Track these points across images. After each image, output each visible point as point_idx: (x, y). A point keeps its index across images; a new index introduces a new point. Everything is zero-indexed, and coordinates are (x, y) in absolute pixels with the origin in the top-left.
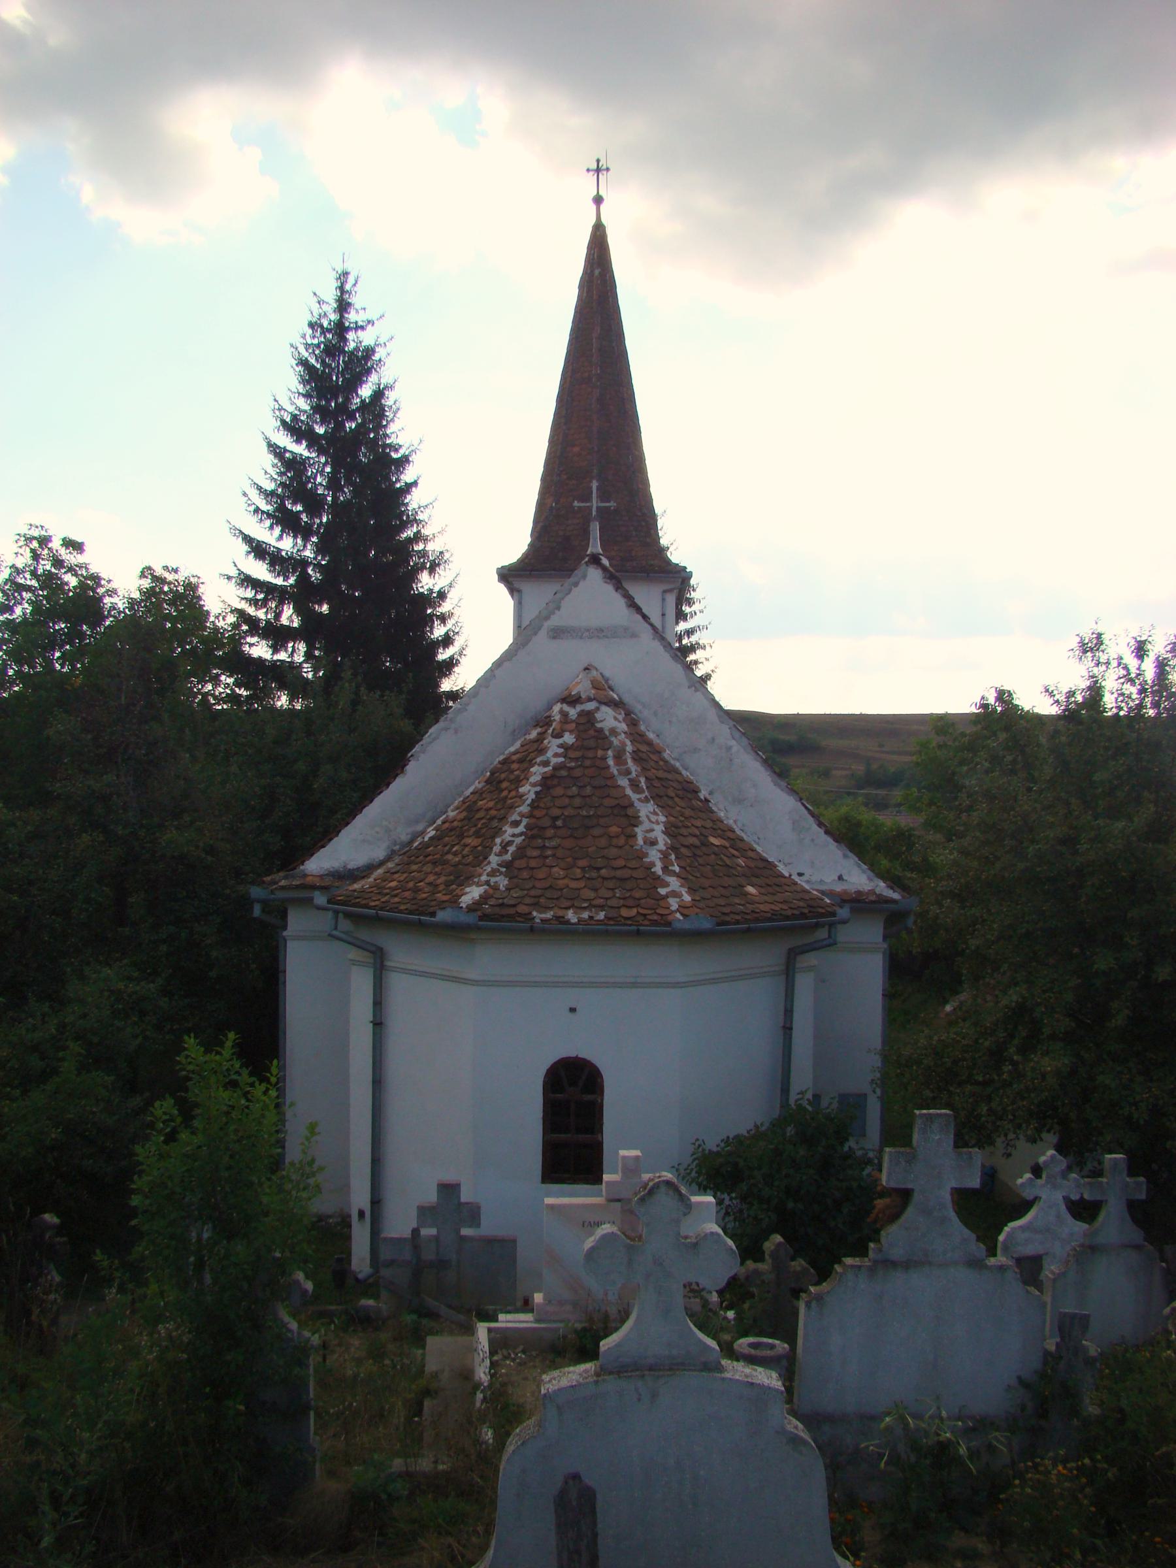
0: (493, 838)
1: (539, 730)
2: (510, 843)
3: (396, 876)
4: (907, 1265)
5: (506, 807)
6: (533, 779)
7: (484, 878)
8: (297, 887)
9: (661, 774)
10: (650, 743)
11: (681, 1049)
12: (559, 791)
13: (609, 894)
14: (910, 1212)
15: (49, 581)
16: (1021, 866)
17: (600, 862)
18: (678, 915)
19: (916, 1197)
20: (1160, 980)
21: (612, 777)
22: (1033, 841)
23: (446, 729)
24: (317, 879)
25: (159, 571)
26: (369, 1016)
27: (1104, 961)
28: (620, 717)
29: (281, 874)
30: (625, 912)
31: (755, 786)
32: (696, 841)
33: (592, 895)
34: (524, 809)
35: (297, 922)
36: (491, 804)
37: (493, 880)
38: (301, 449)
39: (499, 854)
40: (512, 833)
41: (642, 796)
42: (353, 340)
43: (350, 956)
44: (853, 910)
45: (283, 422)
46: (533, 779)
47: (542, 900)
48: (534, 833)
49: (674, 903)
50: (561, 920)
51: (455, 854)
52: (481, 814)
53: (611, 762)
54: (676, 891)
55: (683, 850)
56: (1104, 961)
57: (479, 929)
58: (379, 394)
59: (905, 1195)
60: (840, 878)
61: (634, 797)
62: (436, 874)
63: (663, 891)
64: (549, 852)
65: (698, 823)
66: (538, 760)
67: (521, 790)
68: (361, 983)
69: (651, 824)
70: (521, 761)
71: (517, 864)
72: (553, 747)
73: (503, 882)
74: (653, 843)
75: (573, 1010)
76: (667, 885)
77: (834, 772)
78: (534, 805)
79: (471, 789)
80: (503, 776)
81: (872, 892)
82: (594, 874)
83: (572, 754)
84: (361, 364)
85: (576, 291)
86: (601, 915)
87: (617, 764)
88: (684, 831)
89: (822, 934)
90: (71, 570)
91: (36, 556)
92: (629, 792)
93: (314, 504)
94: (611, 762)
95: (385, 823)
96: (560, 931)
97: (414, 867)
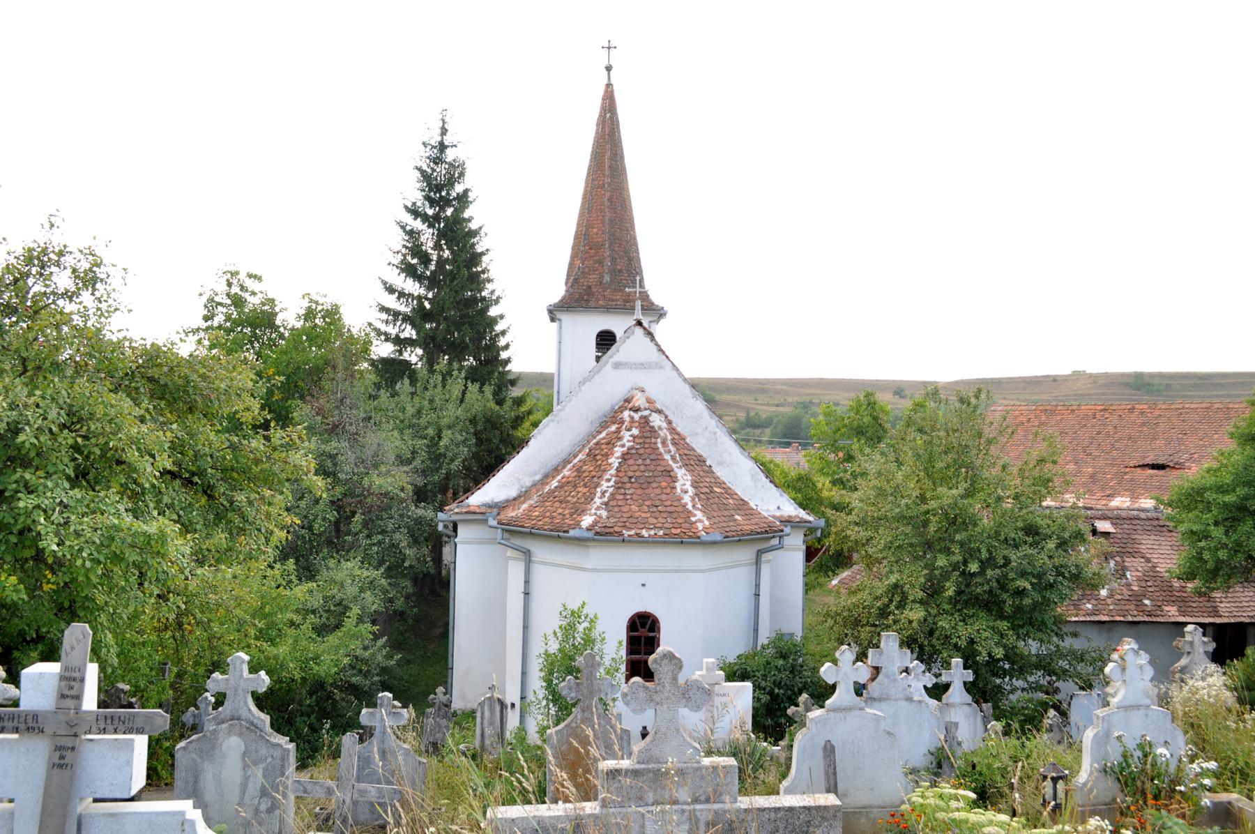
4: (880, 700)
5: (601, 470)
7: (593, 511)
10: (679, 434)
11: (710, 608)
12: (631, 462)
14: (880, 677)
15: (238, 302)
16: (897, 510)
17: (657, 503)
19: (883, 670)
25: (315, 298)
26: (521, 587)
27: (942, 561)
29: (455, 505)
30: (674, 531)
34: (613, 472)
38: (418, 224)
40: (607, 486)
42: (450, 155)
45: (406, 207)
48: (619, 486)
49: (700, 526)
53: (660, 445)
54: (700, 520)
56: (942, 561)
57: (594, 540)
58: (466, 191)
61: (674, 466)
63: (693, 519)
68: (516, 570)
69: (684, 480)
70: (607, 444)
72: (627, 436)
73: (604, 514)
78: (618, 470)
84: (456, 172)
86: (661, 533)
89: (775, 542)
90: (253, 293)
91: (229, 284)
92: (671, 462)
93: (425, 259)
94: (660, 445)
96: (639, 541)
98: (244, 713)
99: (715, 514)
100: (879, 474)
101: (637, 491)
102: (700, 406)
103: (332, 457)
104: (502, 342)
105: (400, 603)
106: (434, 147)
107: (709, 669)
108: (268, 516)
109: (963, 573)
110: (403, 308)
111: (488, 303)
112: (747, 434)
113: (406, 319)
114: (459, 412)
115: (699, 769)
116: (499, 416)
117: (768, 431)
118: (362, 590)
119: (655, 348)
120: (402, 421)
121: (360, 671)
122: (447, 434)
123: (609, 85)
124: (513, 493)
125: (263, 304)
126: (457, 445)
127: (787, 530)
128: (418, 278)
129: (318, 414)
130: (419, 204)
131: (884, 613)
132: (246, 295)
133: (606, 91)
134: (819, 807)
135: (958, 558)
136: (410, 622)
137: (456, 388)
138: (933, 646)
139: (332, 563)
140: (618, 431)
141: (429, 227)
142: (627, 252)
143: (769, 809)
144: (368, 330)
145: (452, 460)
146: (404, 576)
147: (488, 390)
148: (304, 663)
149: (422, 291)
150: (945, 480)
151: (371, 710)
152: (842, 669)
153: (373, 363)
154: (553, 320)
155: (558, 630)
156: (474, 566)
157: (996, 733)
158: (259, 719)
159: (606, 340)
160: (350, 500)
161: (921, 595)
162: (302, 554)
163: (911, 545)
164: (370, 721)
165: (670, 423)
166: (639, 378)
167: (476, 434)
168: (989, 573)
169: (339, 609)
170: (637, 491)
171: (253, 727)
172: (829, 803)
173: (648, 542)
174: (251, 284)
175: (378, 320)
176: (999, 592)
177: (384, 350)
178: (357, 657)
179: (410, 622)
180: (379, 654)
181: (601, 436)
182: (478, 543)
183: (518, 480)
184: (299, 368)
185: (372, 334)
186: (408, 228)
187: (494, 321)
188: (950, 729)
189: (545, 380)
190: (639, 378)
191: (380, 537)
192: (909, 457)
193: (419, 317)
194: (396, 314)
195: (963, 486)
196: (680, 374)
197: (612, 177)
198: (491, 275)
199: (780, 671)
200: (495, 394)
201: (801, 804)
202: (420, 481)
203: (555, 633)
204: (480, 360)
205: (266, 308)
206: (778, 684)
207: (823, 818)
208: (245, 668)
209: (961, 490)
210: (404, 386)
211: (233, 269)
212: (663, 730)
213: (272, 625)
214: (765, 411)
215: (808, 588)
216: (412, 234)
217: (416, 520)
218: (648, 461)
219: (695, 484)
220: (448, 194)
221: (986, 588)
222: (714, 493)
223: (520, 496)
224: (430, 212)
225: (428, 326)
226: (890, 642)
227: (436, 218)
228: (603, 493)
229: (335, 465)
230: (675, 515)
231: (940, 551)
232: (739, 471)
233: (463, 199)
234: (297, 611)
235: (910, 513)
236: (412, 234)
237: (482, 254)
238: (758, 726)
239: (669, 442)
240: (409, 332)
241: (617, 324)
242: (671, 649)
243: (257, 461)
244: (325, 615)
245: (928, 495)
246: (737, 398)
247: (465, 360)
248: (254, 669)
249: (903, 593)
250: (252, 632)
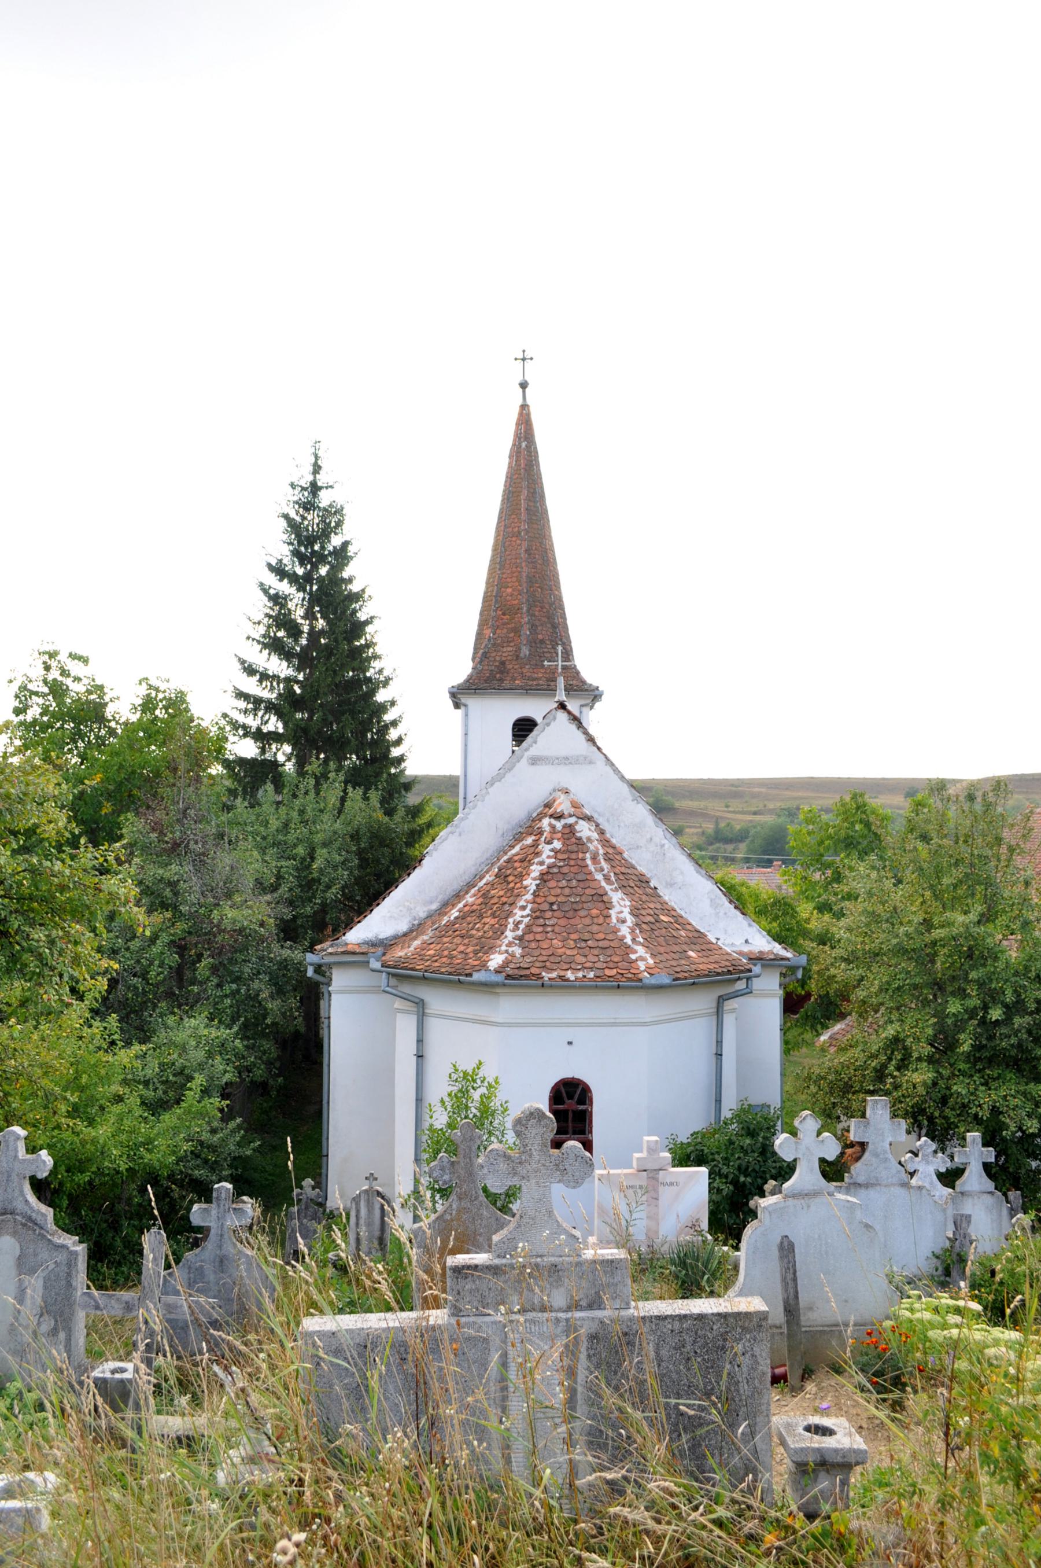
0: (506, 918)
1: (533, 838)
2: (519, 922)
3: (432, 946)
4: (867, 1186)
6: (533, 875)
7: (504, 948)
8: (343, 953)
9: (623, 870)
10: (614, 847)
11: (652, 1069)
12: (552, 884)
13: (596, 959)
14: (867, 1155)
15: (57, 690)
16: (894, 941)
17: (587, 936)
18: (646, 974)
19: (870, 1147)
20: (993, 1019)
21: (591, 873)
22: (901, 924)
23: (452, 833)
24: (356, 947)
25: (153, 682)
27: (954, 1007)
28: (593, 828)
29: (328, 943)
30: (608, 972)
31: (682, 873)
32: (650, 919)
33: (584, 960)
34: (529, 897)
35: (339, 979)
36: (502, 893)
37: (510, 950)
38: (284, 587)
39: (513, 931)
40: (521, 915)
41: (613, 887)
42: (325, 499)
43: (395, 1006)
44: (763, 966)
45: (269, 566)
46: (533, 875)
47: (548, 964)
48: (537, 915)
49: (642, 965)
50: (562, 978)
51: (478, 930)
52: (495, 900)
53: (589, 862)
54: (642, 957)
55: (644, 926)
56: (954, 1007)
57: (504, 985)
58: (346, 544)
59: (863, 1145)
60: (747, 941)
61: (608, 888)
62: (464, 945)
63: (633, 957)
64: (549, 929)
65: (652, 905)
66: (536, 860)
67: (525, 883)
68: (406, 1026)
69: (621, 906)
70: (522, 861)
71: (527, 937)
72: (546, 850)
73: (518, 951)
74: (624, 922)
75: (570, 1043)
76: (636, 952)
77: (687, 830)
78: (535, 894)
79: (484, 881)
80: (509, 872)
81: (771, 952)
82: (583, 945)
83: (560, 856)
84: (332, 520)
85: (507, 460)
86: (591, 975)
87: (594, 863)
88: (643, 912)
89: (741, 985)
90: (77, 679)
91: (47, 668)
92: (603, 884)
93: (294, 631)
94: (589, 862)
95: (407, 904)
96: (562, 985)
97: (445, 940)
98: (19, 1205)
99: (662, 950)
100: (870, 894)
101: (560, 921)
102: (641, 812)
103: (173, 884)
104: (393, 734)
105: (259, 1073)
106: (303, 489)
107: (652, 1150)
108: (76, 960)
109: (983, 1022)
110: (266, 694)
111: (374, 686)
112: (717, 850)
113: (271, 707)
114: (337, 825)
115: (579, 1264)
116: (389, 830)
117: (743, 846)
118: (210, 1055)
119: (583, 737)
120: (264, 838)
121: (206, 1161)
122: (321, 853)
123: (524, 407)
124: (403, 927)
125: (89, 692)
126: (335, 868)
127: (757, 969)
128: (286, 655)
129: (153, 830)
130: (285, 561)
131: (880, 1075)
132: (68, 681)
133: (521, 414)
134: (739, 1314)
135: (974, 1002)
136: (274, 1093)
137: (332, 794)
138: (946, 1118)
139: (171, 1020)
140: (535, 844)
141: (298, 590)
142: (550, 617)
143: (672, 1317)
144: (223, 722)
145: (328, 887)
146: (263, 1035)
147: (375, 796)
148: (132, 1150)
149: (290, 672)
150: (954, 903)
151: (204, 1206)
152: (805, 1143)
153: (227, 764)
154: (457, 706)
155: (447, 1099)
156: (354, 1022)
157: (1023, 1229)
158: (39, 1212)
159: (523, 728)
160: (194, 939)
161: (928, 1050)
162: (130, 1008)
163: (915, 987)
164: (203, 1220)
165: (602, 832)
166: (563, 776)
167: (360, 853)
168: (1017, 1021)
169: (180, 1079)
170: (560, 921)
171: (31, 1223)
172: (751, 1309)
173: (574, 987)
174: (75, 668)
175: (234, 708)
176: (1031, 1046)
177: (247, 749)
178: (201, 1143)
179: (274, 1093)
180: (231, 1137)
181: (514, 851)
182: (358, 992)
183: (409, 909)
184: (133, 772)
185: (228, 728)
186: (272, 592)
187: (382, 708)
188: (961, 1222)
189: (449, 785)
190: (563, 776)
191: (234, 986)
192: (909, 875)
193: (286, 705)
194: (257, 701)
195: (979, 908)
196: (616, 771)
197: (530, 522)
198: (378, 650)
199: (746, 1153)
200: (383, 801)
201: (715, 1311)
202: (287, 913)
203: (442, 1101)
204: (365, 758)
205: (92, 697)
206: (743, 1170)
207: (743, 1328)
208: (21, 1146)
209: (973, 917)
210: (267, 792)
211: (50, 648)
212: (531, 1213)
213: (92, 1100)
214: (739, 821)
215: (788, 1047)
216: (277, 599)
217: (280, 963)
218: (574, 883)
219: (635, 912)
220: (323, 548)
221: (1013, 1040)
222: (660, 922)
223: (411, 931)
224: (300, 571)
225: (299, 715)
226: (878, 1109)
227: (308, 578)
228: (517, 924)
229: (176, 894)
230: (609, 952)
231: (953, 994)
232: (695, 896)
233: (342, 555)
234: (125, 1082)
235: (910, 945)
236: (277, 599)
237: (367, 623)
238: (716, 1223)
239: (601, 858)
240: (274, 724)
241: (534, 708)
242: (527, 1105)
243: (63, 888)
244: (161, 1087)
245: (936, 921)
246: (703, 804)
247: (346, 759)
248: (32, 1149)
249: (905, 1048)
250: (63, 1108)
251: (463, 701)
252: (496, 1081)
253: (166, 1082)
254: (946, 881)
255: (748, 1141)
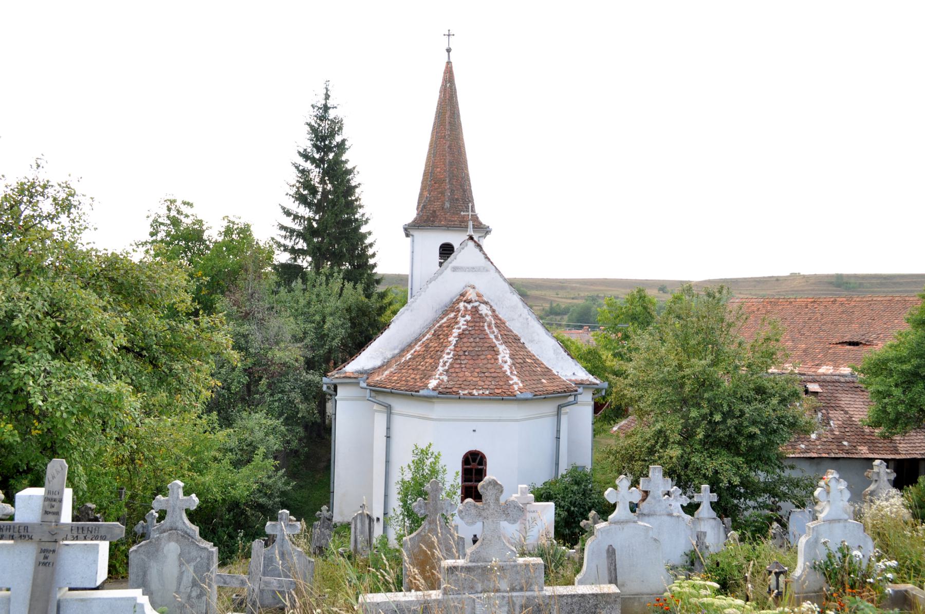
4: (649, 515)
5: (443, 346)
7: (437, 376)
10: (500, 320)
11: (523, 447)
12: (465, 340)
14: (649, 498)
15: (175, 222)
16: (661, 376)
17: (485, 370)
19: (651, 493)
25: (232, 219)
26: (384, 432)
27: (694, 413)
29: (335, 372)
30: (497, 391)
34: (452, 347)
38: (308, 165)
40: (447, 357)
42: (332, 114)
45: (299, 153)
48: (456, 358)
49: (516, 387)
53: (486, 328)
54: (516, 383)
56: (694, 413)
57: (438, 397)
58: (344, 141)
61: (497, 343)
63: (511, 382)
68: (380, 420)
69: (504, 353)
70: (448, 327)
72: (462, 321)
73: (445, 378)
74: (506, 362)
78: (455, 346)
84: (336, 127)
86: (487, 392)
89: (571, 399)
90: (187, 216)
91: (169, 209)
92: (494, 340)
93: (313, 191)
94: (486, 328)
96: (471, 398)
98: (180, 525)
99: (527, 378)
100: (648, 349)
101: (470, 361)
102: (516, 299)
103: (245, 336)
104: (370, 252)
105: (295, 444)
106: (320, 108)
107: (523, 493)
108: (198, 380)
109: (710, 422)
110: (297, 227)
111: (359, 223)
112: (551, 320)
114: (338, 304)
115: (516, 566)
116: (368, 307)
117: (566, 317)
118: (267, 434)
119: (483, 256)
120: (296, 310)
121: (266, 494)
122: (329, 320)
123: (449, 63)
124: (378, 363)
125: (194, 224)
126: (337, 328)
127: (580, 390)
128: (308, 204)
129: (234, 305)
130: (309, 150)
131: (651, 451)
132: (182, 217)
133: (447, 67)
134: (604, 594)
135: (706, 411)
136: (302, 458)
137: (336, 286)
138: (688, 476)
139: (244, 414)
140: (456, 317)
141: (316, 167)
142: (462, 186)
143: (567, 596)
144: (271, 243)
145: (333, 339)
146: (298, 424)
147: (360, 287)
148: (224, 488)
149: (311, 215)
150: (697, 354)
151: (273, 523)
152: (620, 493)
153: (275, 267)
154: (407, 235)
155: (411, 464)
156: (349, 417)
157: (734, 540)
158: (191, 529)
159: (446, 251)
160: (258, 368)
161: (678, 438)
162: (223, 408)
163: (672, 401)
165: (494, 311)
166: (471, 278)
167: (351, 319)
168: (729, 422)
169: (250, 448)
170: (470, 361)
171: (187, 535)
172: (611, 592)
173: (477, 399)
174: (185, 209)
175: (279, 235)
176: (736, 436)
177: (283, 258)
178: (263, 484)
179: (302, 458)
180: (280, 481)
181: (443, 321)
182: (352, 400)
183: (382, 353)
184: (220, 271)
185: (274, 246)
186: (301, 168)
187: (364, 236)
188: (700, 536)
189: (402, 280)
190: (471, 278)
191: (280, 395)
192: (670, 337)
193: (309, 233)
194: (292, 231)
195: (710, 358)
196: (501, 276)
197: (451, 130)
198: (362, 202)
199: (575, 494)
200: (365, 290)
201: (591, 592)
202: (310, 354)
203: (409, 466)
204: (354, 265)
205: (196, 226)
206: (573, 504)
207: (606, 602)
208: (181, 492)
209: (708, 361)
210: (298, 284)
211: (172, 198)
212: (489, 538)
213: (200, 460)
214: (564, 303)
215: (595, 433)
216: (303, 172)
217: (306, 383)
218: (478, 340)
219: (512, 357)
220: (330, 143)
221: (727, 433)
222: (527, 363)
223: (383, 365)
224: (317, 156)
225: (315, 240)
226: (656, 472)
227: (322, 160)
228: (445, 363)
229: (247, 342)
230: (497, 379)
231: (693, 406)
232: (544, 347)
233: (341, 147)
234: (219, 450)
235: (670, 378)
236: (303, 172)
237: (356, 187)
238: (559, 534)
239: (493, 326)
240: (301, 245)
241: (455, 238)
242: (494, 478)
243: (190, 340)
244: (239, 453)
245: (684, 364)
246: (543, 293)
248: (187, 493)
249: (666, 436)
250: (186, 465)
251: (412, 232)
252: (439, 454)
253: (242, 450)
254: (693, 342)
255: (576, 487)
